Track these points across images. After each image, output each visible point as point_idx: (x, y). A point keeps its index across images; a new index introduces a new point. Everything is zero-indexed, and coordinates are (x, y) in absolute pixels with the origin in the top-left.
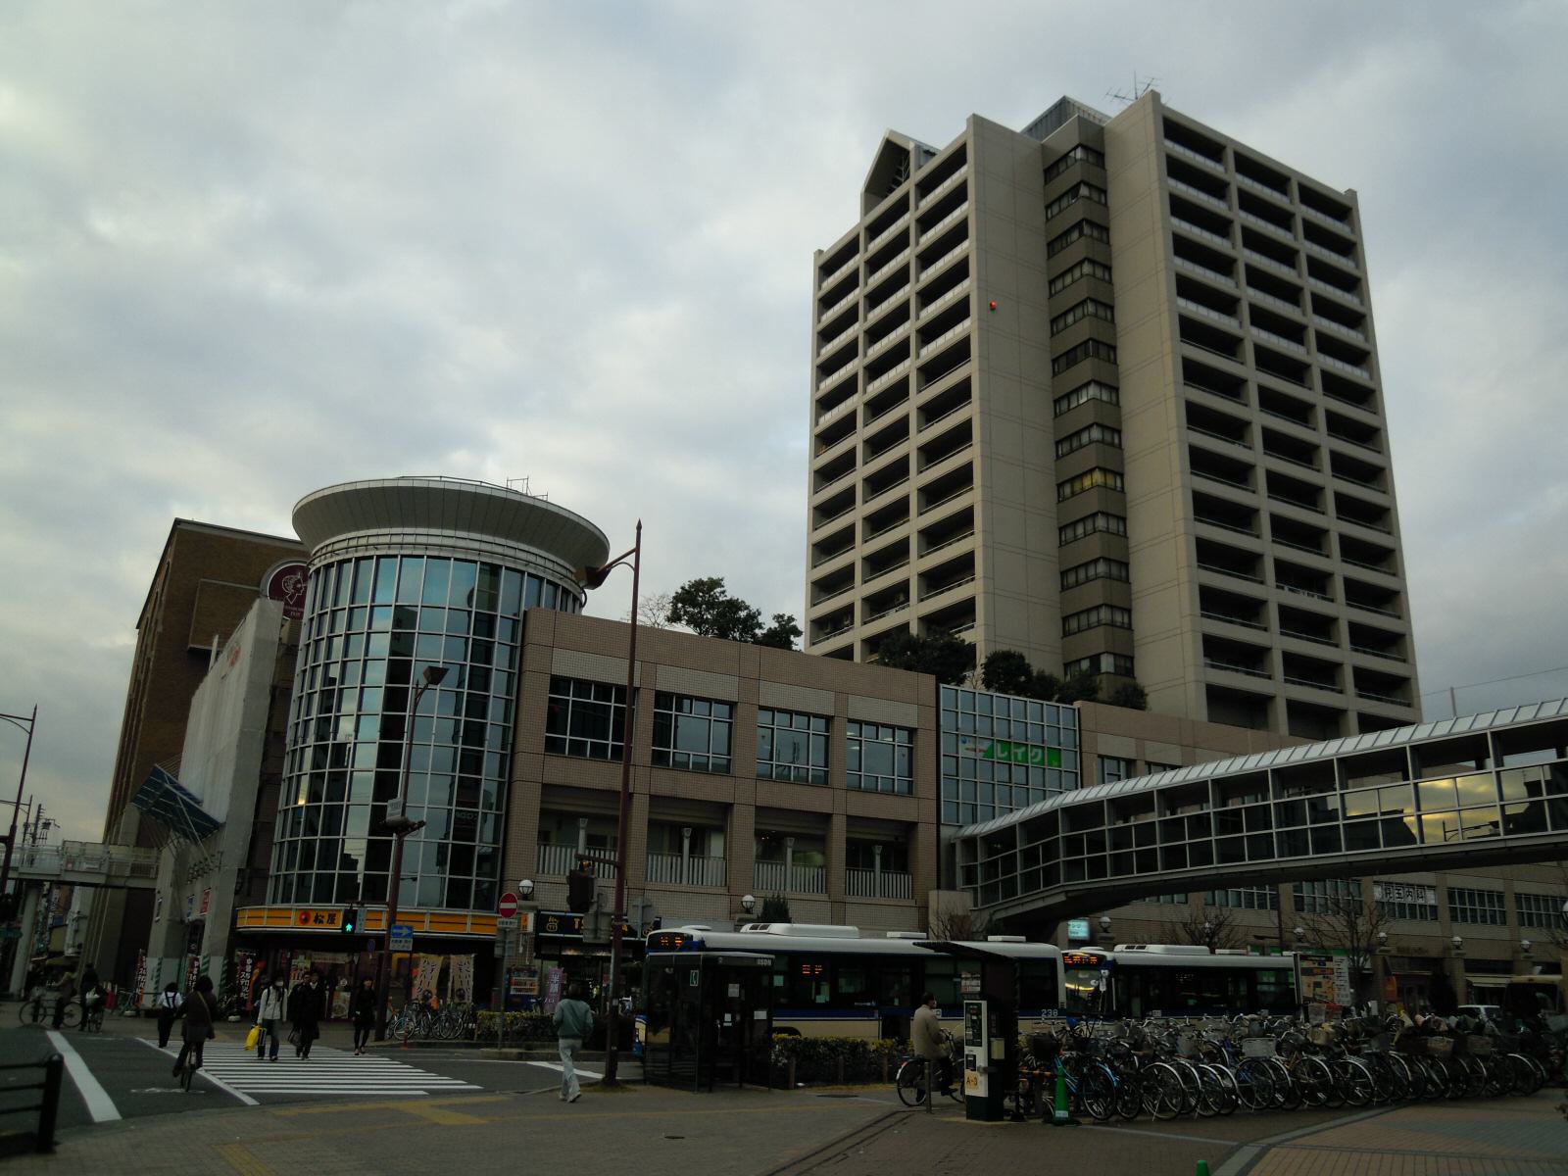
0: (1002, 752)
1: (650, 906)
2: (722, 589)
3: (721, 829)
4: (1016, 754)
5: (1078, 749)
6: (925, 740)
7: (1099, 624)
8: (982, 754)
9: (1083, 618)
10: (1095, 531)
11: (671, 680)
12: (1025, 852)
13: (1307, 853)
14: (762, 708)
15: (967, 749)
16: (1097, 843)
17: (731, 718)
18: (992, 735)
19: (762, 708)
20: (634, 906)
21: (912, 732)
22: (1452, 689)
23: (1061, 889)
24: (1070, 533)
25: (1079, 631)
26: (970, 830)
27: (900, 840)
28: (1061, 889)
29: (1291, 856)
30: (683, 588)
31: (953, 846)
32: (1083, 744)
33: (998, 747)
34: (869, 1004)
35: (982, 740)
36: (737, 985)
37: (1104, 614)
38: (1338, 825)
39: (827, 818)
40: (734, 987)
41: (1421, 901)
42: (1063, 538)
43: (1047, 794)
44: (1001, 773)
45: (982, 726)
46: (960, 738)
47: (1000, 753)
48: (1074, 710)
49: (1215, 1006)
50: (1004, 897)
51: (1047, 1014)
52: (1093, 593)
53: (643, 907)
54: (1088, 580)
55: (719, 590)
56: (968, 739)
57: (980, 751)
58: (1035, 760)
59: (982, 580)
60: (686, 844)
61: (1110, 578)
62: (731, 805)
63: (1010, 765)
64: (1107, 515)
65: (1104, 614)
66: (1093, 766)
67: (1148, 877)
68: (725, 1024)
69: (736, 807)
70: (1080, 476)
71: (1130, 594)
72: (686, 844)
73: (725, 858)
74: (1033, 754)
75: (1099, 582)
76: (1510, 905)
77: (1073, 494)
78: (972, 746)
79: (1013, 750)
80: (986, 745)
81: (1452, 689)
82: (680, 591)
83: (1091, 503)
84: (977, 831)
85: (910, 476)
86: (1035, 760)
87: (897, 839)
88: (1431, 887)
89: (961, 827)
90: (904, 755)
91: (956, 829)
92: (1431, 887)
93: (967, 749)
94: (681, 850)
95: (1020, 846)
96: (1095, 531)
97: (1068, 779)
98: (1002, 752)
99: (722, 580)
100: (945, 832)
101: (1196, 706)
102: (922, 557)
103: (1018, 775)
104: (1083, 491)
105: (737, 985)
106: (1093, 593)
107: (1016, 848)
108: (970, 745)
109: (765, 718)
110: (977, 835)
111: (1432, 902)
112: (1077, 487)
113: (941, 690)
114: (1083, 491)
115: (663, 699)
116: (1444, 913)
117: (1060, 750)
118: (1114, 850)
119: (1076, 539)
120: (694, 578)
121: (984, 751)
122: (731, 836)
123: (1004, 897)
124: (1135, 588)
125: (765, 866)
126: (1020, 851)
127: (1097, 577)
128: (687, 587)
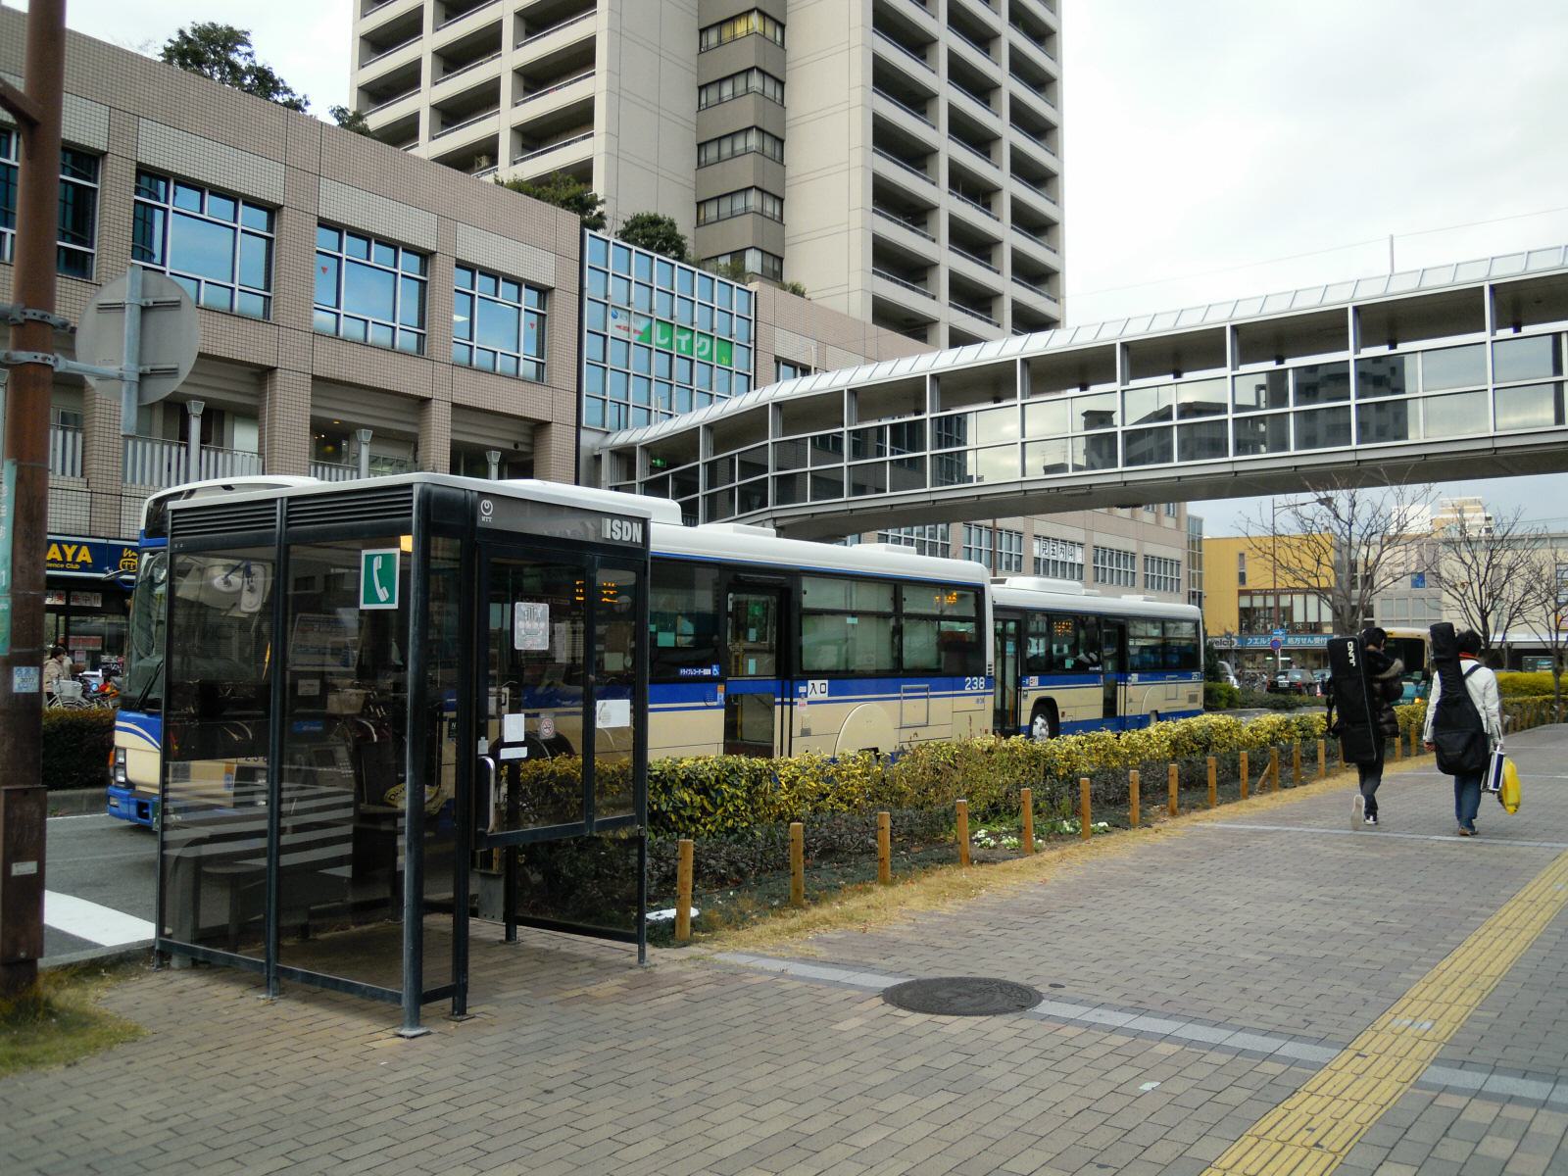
0: (662, 338)
1: (175, 305)
2: (248, 50)
3: (251, 415)
4: (679, 342)
5: (752, 345)
6: (563, 307)
7: (746, 211)
8: (637, 336)
9: (725, 205)
10: (747, 91)
11: (162, 149)
12: (711, 466)
13: (1170, 460)
14: (324, 223)
15: (619, 327)
16: (829, 446)
17: (271, 231)
18: (651, 311)
19: (324, 223)
20: (104, 308)
21: (544, 292)
22: (1392, 238)
23: (768, 516)
24: (713, 93)
25: (719, 220)
26: (621, 438)
27: (521, 448)
28: (768, 516)
29: (1103, 468)
30: (181, 32)
31: (598, 458)
32: (758, 339)
33: (657, 329)
34: (707, 672)
35: (636, 317)
36: (542, 609)
37: (753, 199)
38: (1226, 420)
39: (421, 404)
40: (531, 616)
41: (1070, 559)
42: (703, 101)
43: (715, 398)
44: (659, 364)
45: (639, 302)
46: (610, 310)
47: (659, 339)
48: (750, 293)
49: (683, 672)
50: (740, 512)
51: (972, 685)
52: (743, 171)
53: (145, 309)
54: (734, 155)
55: (242, 49)
56: (619, 312)
57: (635, 331)
58: (700, 353)
59: (604, 136)
60: (195, 427)
61: (763, 154)
62: (272, 370)
63: (671, 355)
64: (763, 73)
65: (753, 199)
66: (767, 366)
67: (869, 501)
68: (506, 754)
69: (279, 374)
70: (732, 19)
71: (784, 180)
72: (195, 427)
73: (260, 454)
74: (700, 344)
75: (750, 158)
76: (1139, 561)
77: (720, 43)
78: (623, 322)
79: (676, 336)
80: (642, 325)
81: (1392, 238)
82: (176, 38)
83: (745, 55)
84: (633, 439)
85: (420, 142)
86: (700, 353)
87: (516, 446)
88: (1080, 545)
89: (608, 433)
90: (532, 325)
91: (600, 436)
92: (1080, 545)
93: (619, 327)
94: (184, 436)
95: (704, 457)
96: (747, 91)
97: (738, 381)
98: (662, 338)
99: (247, 33)
100: (588, 440)
101: (863, 311)
102: (517, 105)
103: (680, 368)
104: (734, 39)
105: (542, 609)
106: (743, 171)
107: (698, 460)
108: (623, 322)
109: (327, 240)
110: (636, 443)
111: (1079, 561)
112: (727, 33)
113: (588, 238)
114: (734, 39)
115: (149, 177)
116: (1089, 572)
117: (731, 343)
118: (854, 460)
119: (721, 101)
120: (203, 20)
121: (640, 333)
122: (272, 427)
123: (740, 512)
124: (790, 172)
125: (327, 469)
126: (704, 464)
127: (746, 152)
128: (189, 34)
